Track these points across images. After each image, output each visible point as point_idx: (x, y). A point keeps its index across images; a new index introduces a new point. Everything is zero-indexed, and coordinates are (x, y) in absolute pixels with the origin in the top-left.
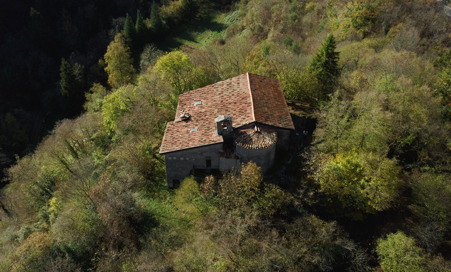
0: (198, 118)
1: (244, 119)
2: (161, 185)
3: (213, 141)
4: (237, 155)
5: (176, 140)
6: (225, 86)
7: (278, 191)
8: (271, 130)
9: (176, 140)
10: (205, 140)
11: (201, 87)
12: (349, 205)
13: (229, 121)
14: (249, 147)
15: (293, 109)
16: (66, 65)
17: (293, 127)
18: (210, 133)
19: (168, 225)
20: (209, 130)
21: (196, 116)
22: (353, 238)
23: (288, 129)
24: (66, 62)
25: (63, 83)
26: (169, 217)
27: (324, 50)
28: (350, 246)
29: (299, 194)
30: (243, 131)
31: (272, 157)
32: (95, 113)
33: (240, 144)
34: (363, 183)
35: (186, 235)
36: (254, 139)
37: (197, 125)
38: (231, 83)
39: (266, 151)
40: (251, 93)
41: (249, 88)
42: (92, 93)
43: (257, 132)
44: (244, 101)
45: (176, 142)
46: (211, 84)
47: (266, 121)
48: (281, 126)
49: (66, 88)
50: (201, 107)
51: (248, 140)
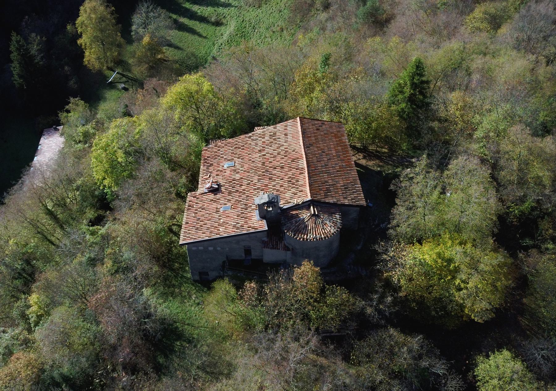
0: (230, 189)
1: (295, 194)
2: (182, 277)
3: (253, 228)
4: (287, 245)
5: (202, 223)
6: (267, 138)
7: (344, 296)
8: (333, 210)
9: (202, 223)
10: (242, 226)
11: (232, 137)
12: (440, 314)
13: (274, 202)
14: (304, 239)
15: (364, 158)
16: (18, 42)
17: (363, 203)
18: (249, 215)
19: (195, 336)
20: (246, 209)
21: (227, 185)
22: (446, 354)
23: (357, 206)
24: (19, 38)
25: (16, 68)
26: (197, 325)
27: (407, 79)
28: (440, 369)
29: (371, 300)
30: (294, 212)
31: (336, 245)
32: (76, 146)
33: (289, 234)
34: (459, 283)
35: (221, 350)
36: (310, 225)
37: (229, 200)
38: (275, 134)
39: (328, 242)
40: (304, 153)
41: (302, 144)
42: (68, 111)
43: (314, 215)
44: (294, 165)
45: (201, 226)
46: (247, 133)
47: (326, 196)
48: (346, 202)
49: (20, 77)
50: (235, 171)
51: (301, 228)
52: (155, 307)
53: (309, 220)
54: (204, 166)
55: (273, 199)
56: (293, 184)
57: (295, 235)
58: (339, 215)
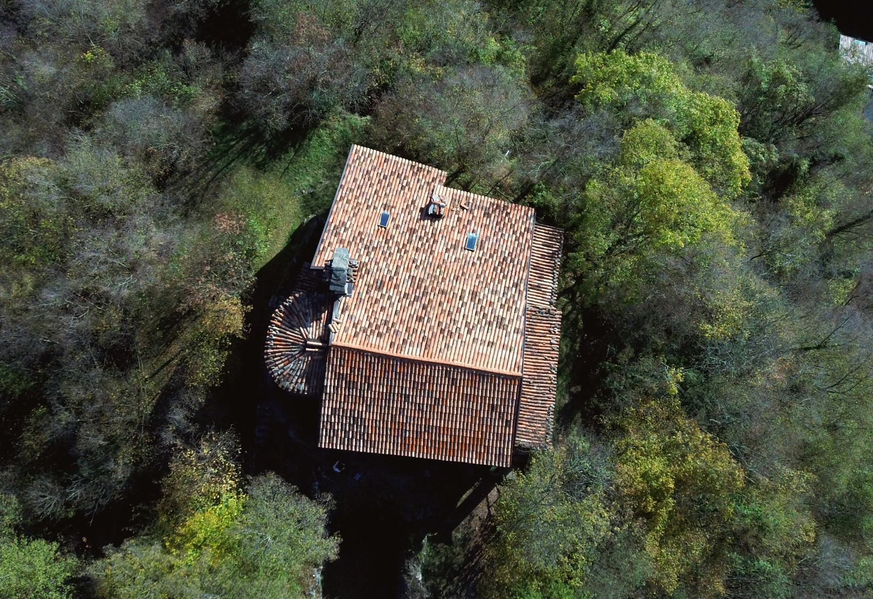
1: (355, 326)
30: (324, 316)
48: (326, 411)
51: (294, 319)
52: (326, 126)
53: (302, 335)
54: (492, 204)
55: (336, 276)
56: (378, 327)
57: (285, 306)
58: (304, 391)
